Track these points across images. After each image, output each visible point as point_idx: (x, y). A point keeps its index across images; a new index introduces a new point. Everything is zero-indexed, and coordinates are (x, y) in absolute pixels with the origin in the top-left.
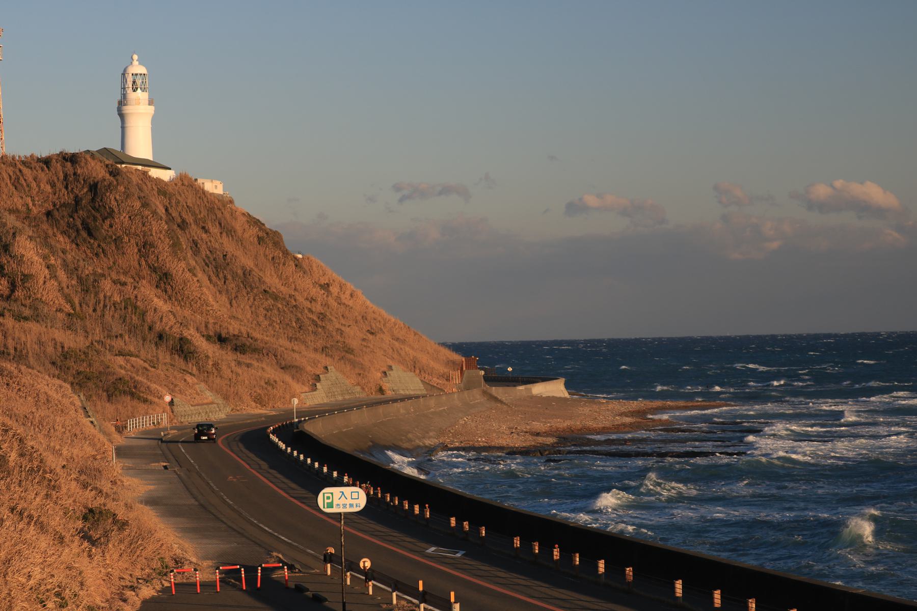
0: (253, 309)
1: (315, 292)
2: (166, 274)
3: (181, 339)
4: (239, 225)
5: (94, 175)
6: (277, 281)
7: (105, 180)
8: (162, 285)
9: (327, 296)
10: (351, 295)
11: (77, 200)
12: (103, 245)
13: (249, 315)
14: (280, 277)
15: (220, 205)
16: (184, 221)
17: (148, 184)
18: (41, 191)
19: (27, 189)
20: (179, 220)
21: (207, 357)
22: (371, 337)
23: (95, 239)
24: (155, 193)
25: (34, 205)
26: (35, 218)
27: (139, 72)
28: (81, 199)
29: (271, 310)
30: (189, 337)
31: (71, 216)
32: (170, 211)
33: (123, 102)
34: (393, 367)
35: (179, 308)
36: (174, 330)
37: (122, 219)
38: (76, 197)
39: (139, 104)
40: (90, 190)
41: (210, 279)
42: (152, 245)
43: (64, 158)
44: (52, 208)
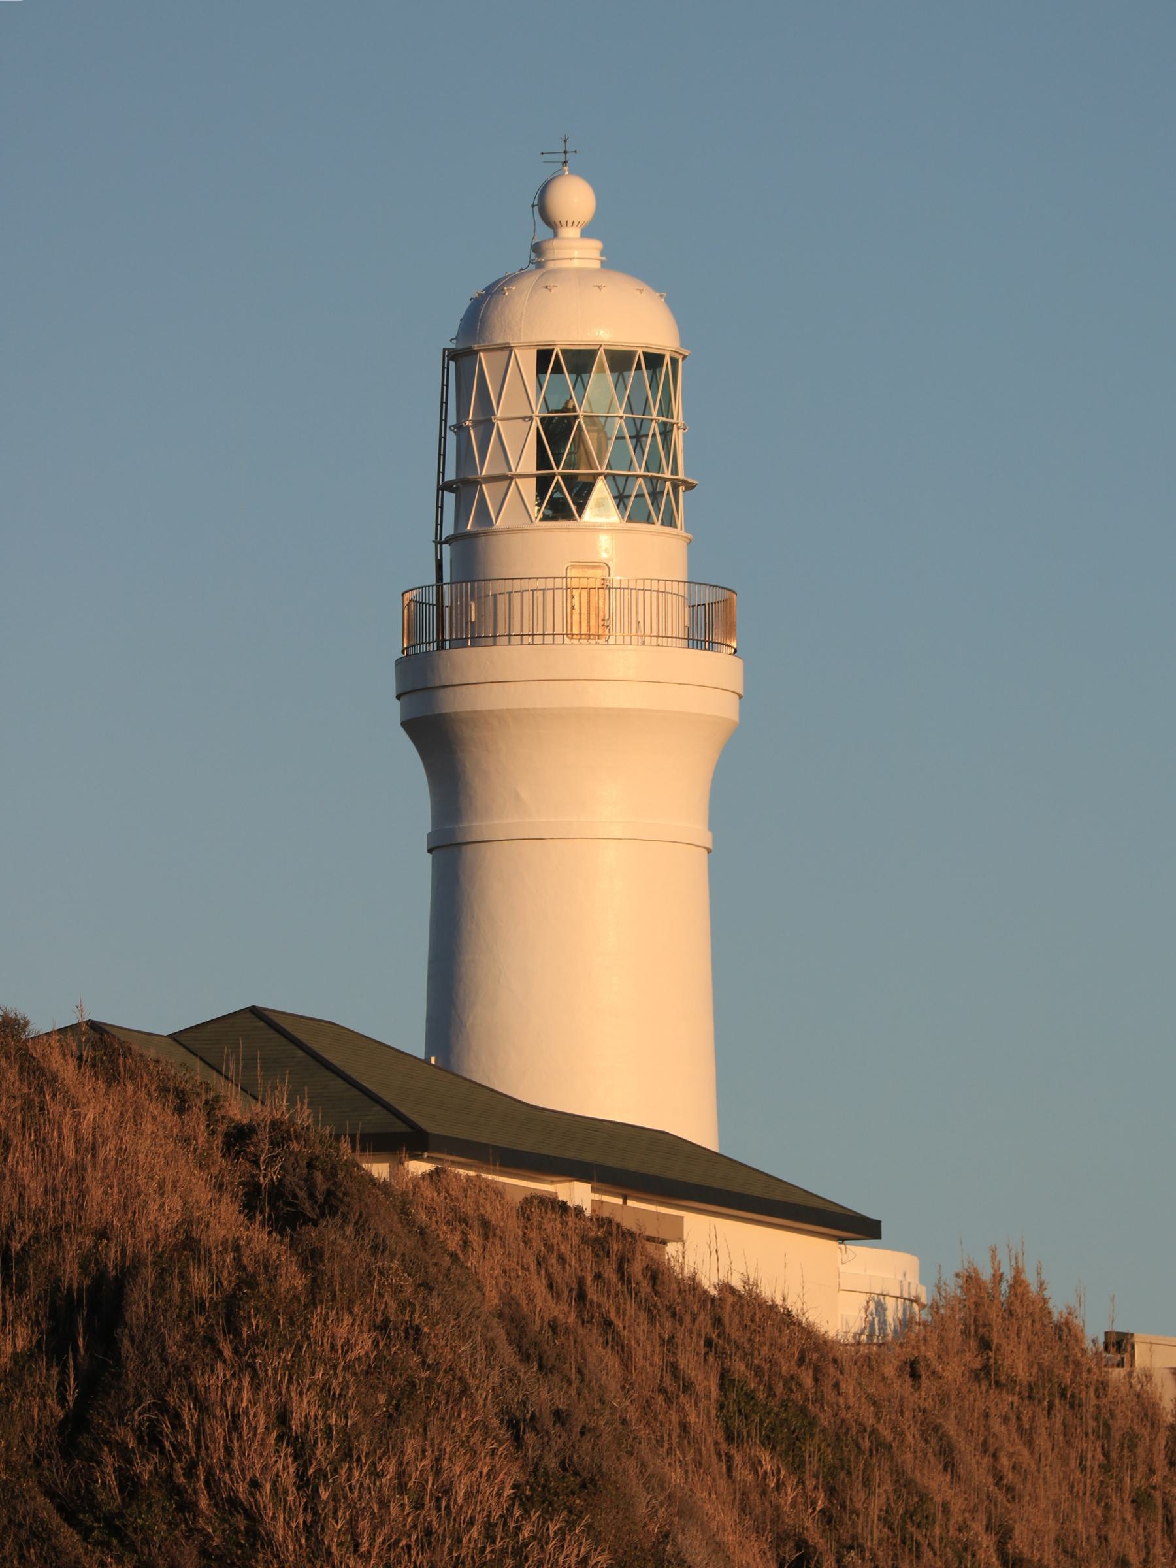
7: (188, 1245)
24: (701, 1416)
27: (603, 334)
33: (456, 608)
40: (55, 1342)
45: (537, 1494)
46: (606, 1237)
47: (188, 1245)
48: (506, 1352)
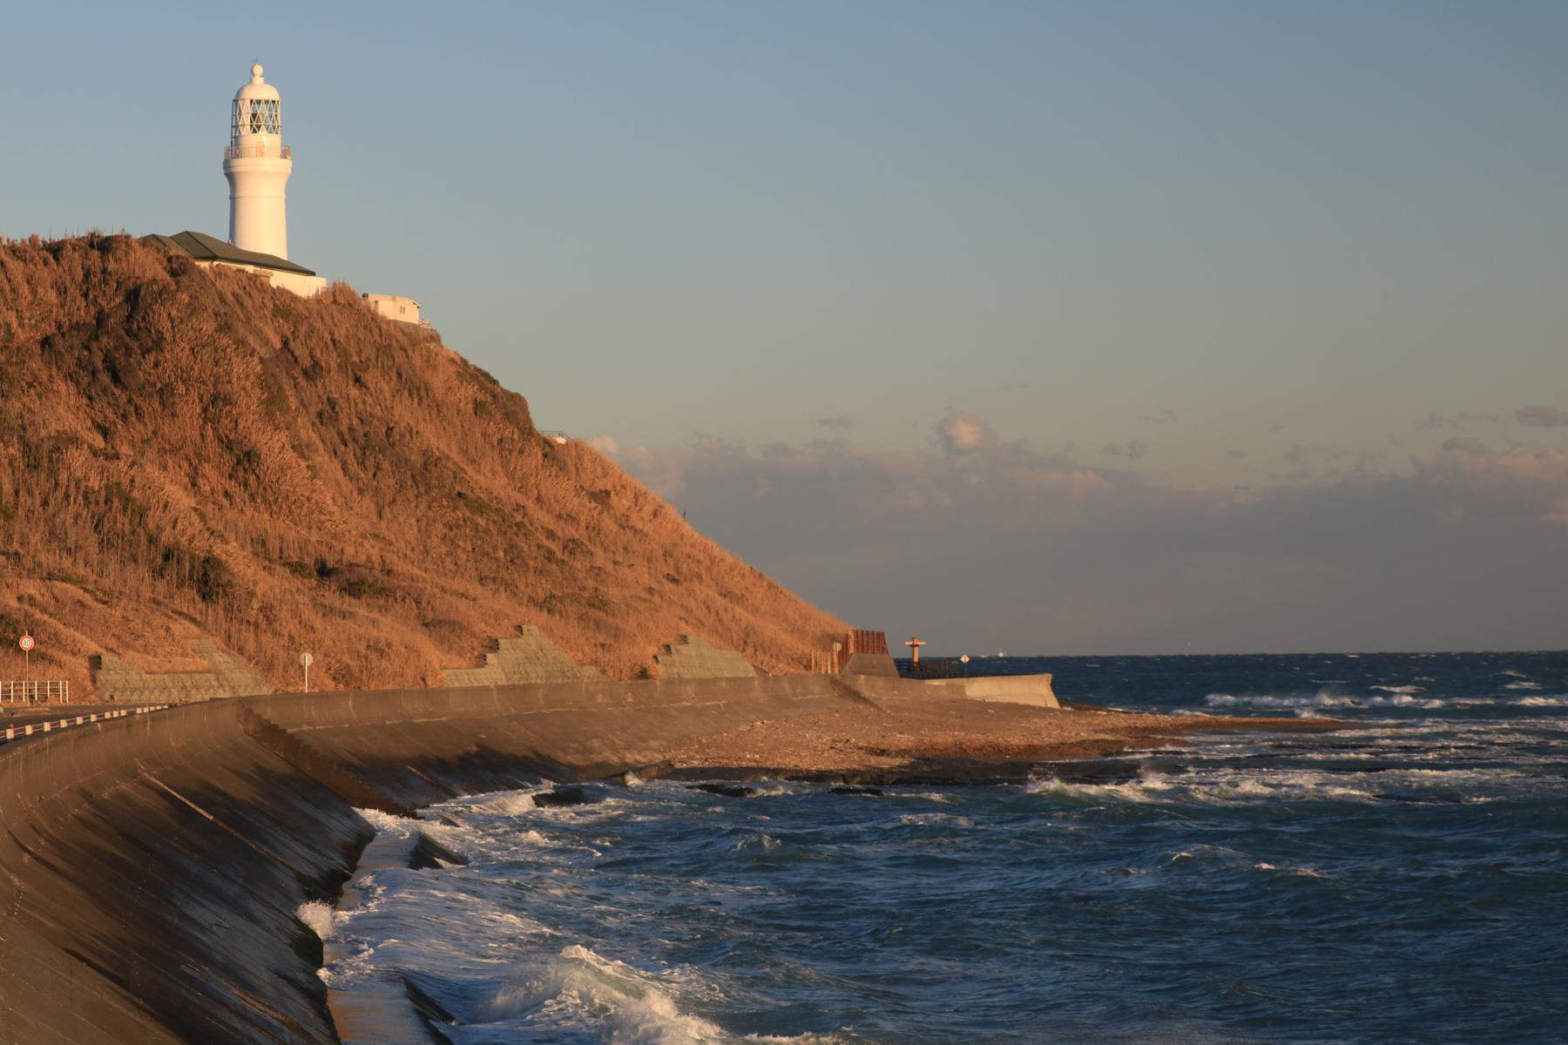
0: (423, 524)
1: (585, 508)
2: (248, 454)
3: (207, 560)
4: (438, 382)
5: (138, 272)
6: (504, 481)
8: (241, 474)
9: (601, 513)
10: (655, 514)
11: (101, 319)
12: (138, 400)
13: (412, 535)
14: (510, 476)
15: (405, 342)
16: (316, 364)
17: (255, 294)
18: (36, 301)
19: (10, 296)
20: (307, 363)
21: (251, 594)
22: (668, 586)
23: (125, 388)
25: (21, 325)
26: (19, 349)
28: (109, 315)
29: (458, 527)
30: (224, 557)
31: (88, 348)
32: (292, 345)
33: (235, 149)
34: (690, 638)
35: (266, 516)
36: (196, 543)
37: (178, 353)
38: (101, 311)
39: (262, 154)
40: (127, 299)
41: (344, 468)
42: (228, 401)
43: (92, 246)
44: (54, 330)
45: (219, 329)
46: (253, 278)
47: (154, 280)
48: (217, 300)
